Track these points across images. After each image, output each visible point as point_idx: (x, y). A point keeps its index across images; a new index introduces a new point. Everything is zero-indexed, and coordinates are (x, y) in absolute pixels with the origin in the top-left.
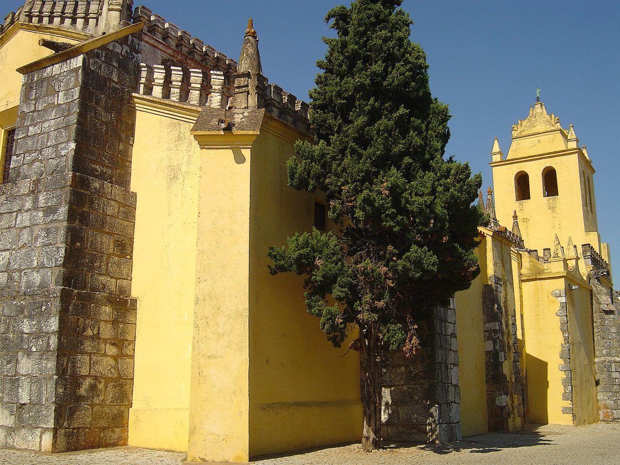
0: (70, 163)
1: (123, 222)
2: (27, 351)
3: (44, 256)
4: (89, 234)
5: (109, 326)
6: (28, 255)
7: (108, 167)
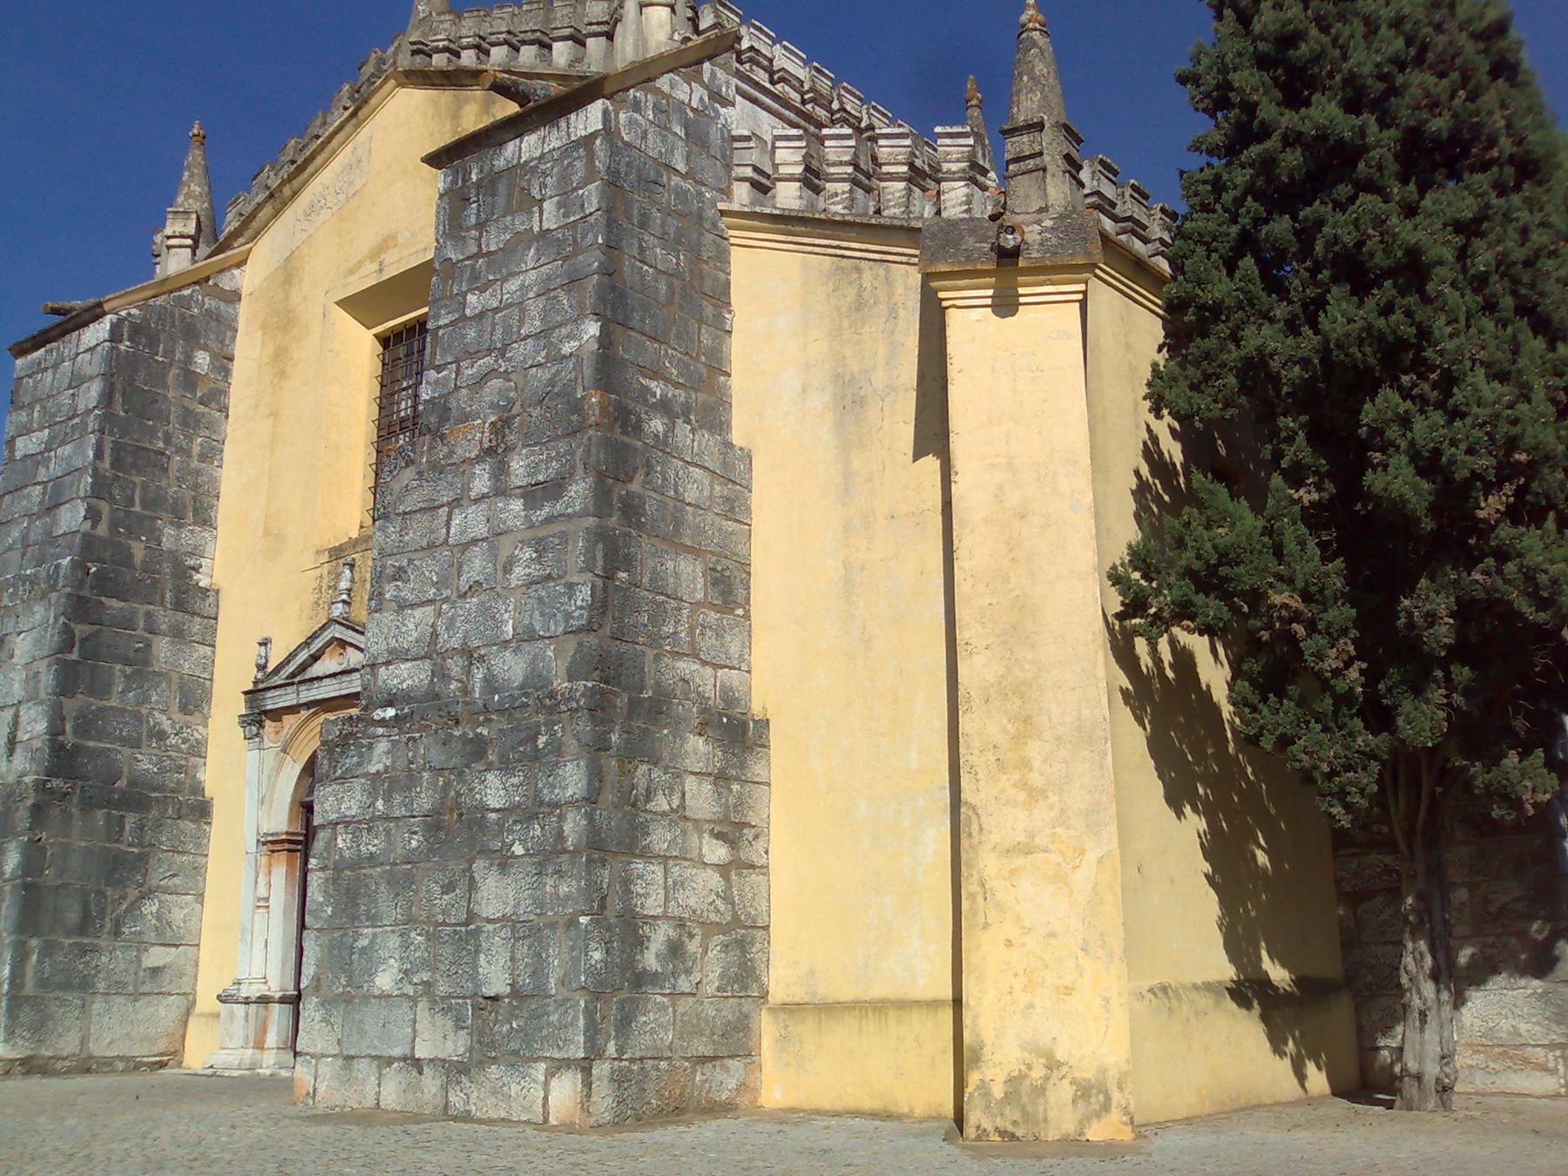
0: (588, 371)
1: (724, 523)
2: (498, 854)
3: (533, 610)
4: (644, 547)
5: (707, 787)
6: (486, 612)
7: (677, 385)
